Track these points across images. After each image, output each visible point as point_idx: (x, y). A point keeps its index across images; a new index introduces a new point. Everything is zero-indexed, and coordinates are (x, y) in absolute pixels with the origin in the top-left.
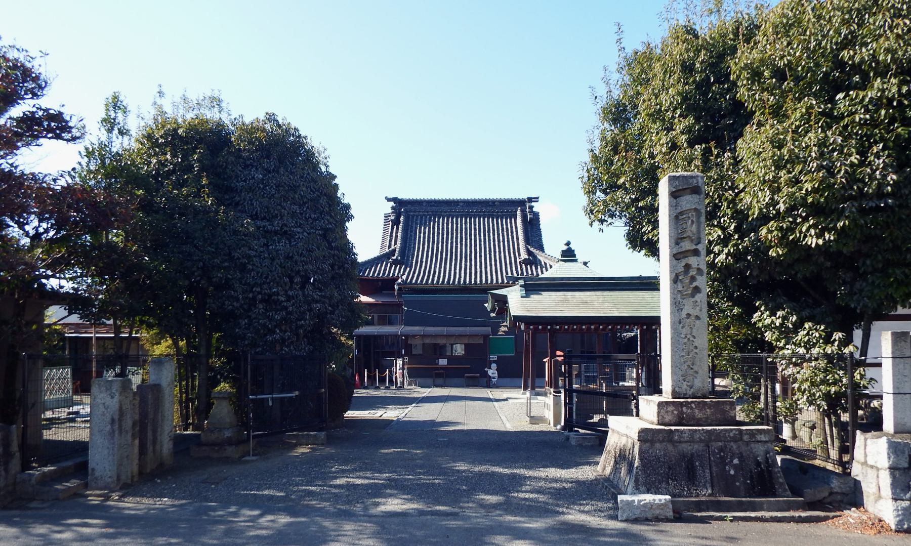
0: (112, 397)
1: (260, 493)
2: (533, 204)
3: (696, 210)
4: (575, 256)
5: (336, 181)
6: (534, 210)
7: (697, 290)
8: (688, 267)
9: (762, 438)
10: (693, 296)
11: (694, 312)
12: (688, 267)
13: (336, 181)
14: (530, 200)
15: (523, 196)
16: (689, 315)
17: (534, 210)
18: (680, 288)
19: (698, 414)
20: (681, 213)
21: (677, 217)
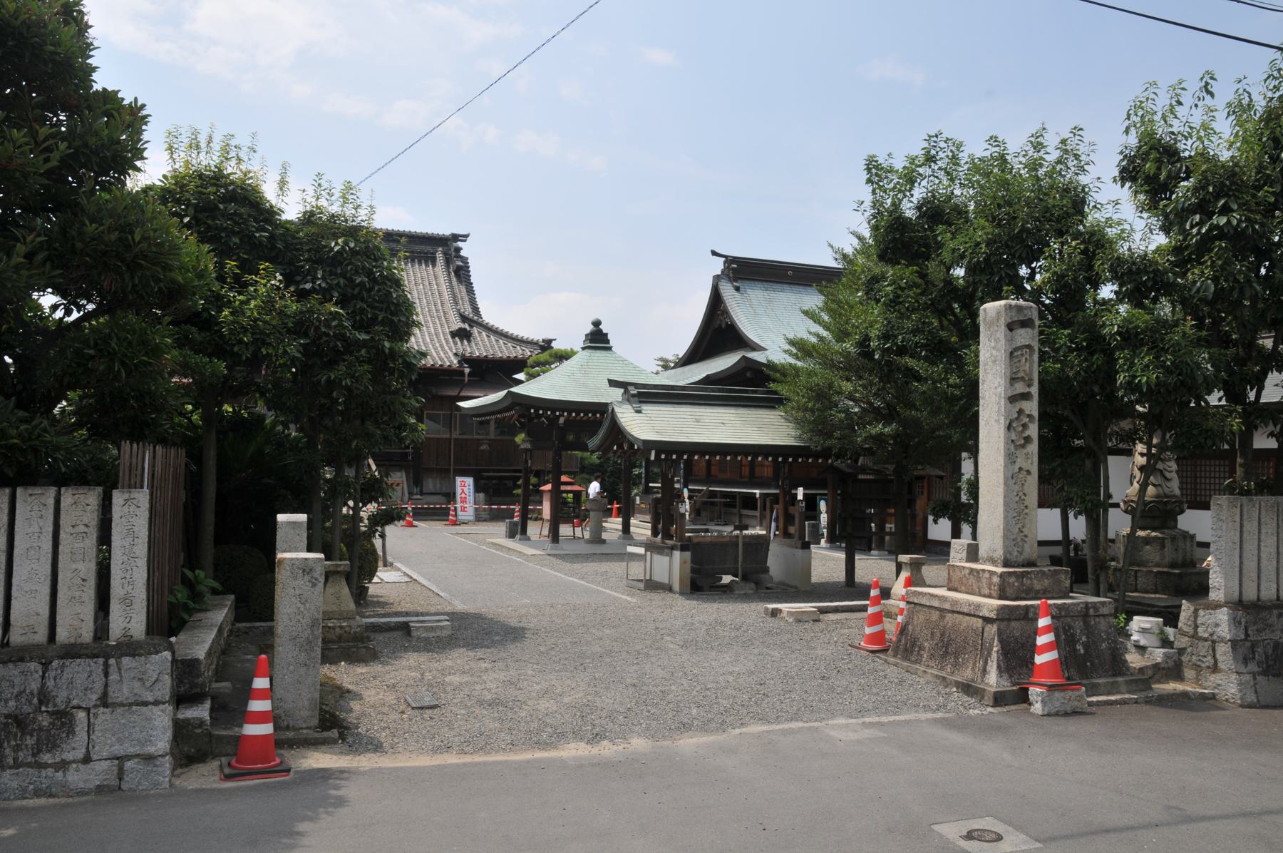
0: (314, 585)
1: (553, 754)
2: (460, 244)
3: (1029, 346)
4: (608, 342)
5: (120, 95)
6: (462, 253)
7: (1028, 440)
8: (1020, 412)
9: (1105, 611)
10: (1023, 446)
11: (1025, 466)
12: (1020, 412)
13: (120, 95)
14: (455, 238)
15: (444, 230)
16: (1020, 469)
17: (462, 253)
18: (1014, 437)
19: (1037, 586)
20: (1016, 349)
21: (1011, 353)
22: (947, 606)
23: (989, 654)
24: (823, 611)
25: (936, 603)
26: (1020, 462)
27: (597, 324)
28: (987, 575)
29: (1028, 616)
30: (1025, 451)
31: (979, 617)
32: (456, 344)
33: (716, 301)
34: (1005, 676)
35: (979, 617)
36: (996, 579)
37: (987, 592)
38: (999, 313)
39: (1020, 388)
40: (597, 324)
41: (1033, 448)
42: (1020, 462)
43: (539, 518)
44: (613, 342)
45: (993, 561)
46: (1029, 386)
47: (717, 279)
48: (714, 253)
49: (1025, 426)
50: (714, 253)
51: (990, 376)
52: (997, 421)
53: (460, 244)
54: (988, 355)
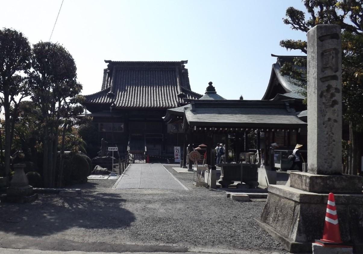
3: (335, 49)
7: (335, 103)
8: (329, 87)
12: (329, 87)
14: (183, 62)
19: (337, 185)
20: (325, 51)
22: (282, 194)
23: (295, 223)
24: (251, 197)
25: (278, 193)
26: (329, 115)
27: (211, 83)
28: (305, 178)
29: (322, 202)
30: (333, 109)
31: (293, 200)
32: (179, 100)
33: (274, 77)
34: (303, 235)
35: (293, 200)
36: (308, 180)
37: (304, 187)
38: (314, 32)
39: (329, 73)
40: (211, 83)
41: (338, 107)
42: (329, 115)
43: (304, 180)
44: (241, 96)
45: (312, 170)
46: (336, 71)
47: (275, 65)
48: (273, 55)
49: (333, 95)
50: (273, 55)
51: (311, 68)
52: (314, 92)
53: (184, 64)
54: (310, 57)
